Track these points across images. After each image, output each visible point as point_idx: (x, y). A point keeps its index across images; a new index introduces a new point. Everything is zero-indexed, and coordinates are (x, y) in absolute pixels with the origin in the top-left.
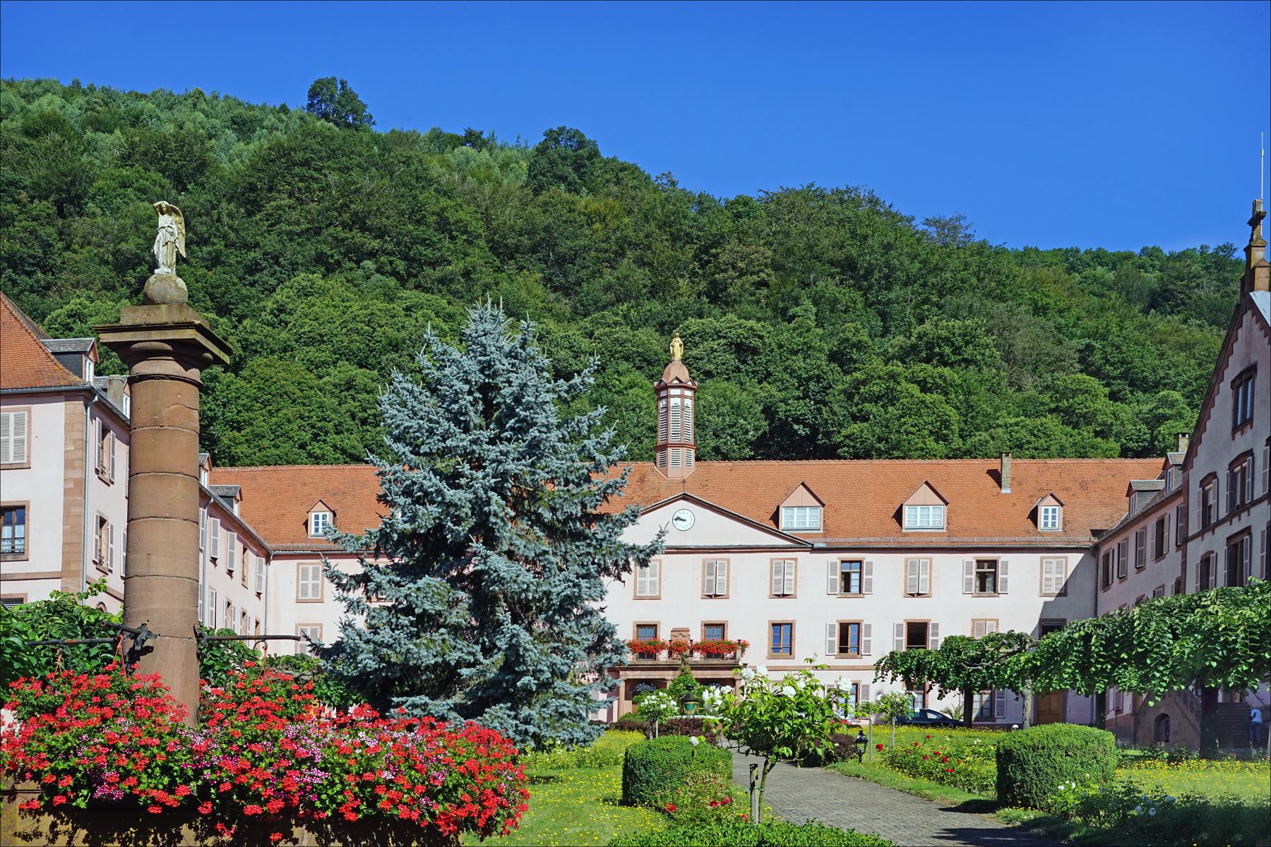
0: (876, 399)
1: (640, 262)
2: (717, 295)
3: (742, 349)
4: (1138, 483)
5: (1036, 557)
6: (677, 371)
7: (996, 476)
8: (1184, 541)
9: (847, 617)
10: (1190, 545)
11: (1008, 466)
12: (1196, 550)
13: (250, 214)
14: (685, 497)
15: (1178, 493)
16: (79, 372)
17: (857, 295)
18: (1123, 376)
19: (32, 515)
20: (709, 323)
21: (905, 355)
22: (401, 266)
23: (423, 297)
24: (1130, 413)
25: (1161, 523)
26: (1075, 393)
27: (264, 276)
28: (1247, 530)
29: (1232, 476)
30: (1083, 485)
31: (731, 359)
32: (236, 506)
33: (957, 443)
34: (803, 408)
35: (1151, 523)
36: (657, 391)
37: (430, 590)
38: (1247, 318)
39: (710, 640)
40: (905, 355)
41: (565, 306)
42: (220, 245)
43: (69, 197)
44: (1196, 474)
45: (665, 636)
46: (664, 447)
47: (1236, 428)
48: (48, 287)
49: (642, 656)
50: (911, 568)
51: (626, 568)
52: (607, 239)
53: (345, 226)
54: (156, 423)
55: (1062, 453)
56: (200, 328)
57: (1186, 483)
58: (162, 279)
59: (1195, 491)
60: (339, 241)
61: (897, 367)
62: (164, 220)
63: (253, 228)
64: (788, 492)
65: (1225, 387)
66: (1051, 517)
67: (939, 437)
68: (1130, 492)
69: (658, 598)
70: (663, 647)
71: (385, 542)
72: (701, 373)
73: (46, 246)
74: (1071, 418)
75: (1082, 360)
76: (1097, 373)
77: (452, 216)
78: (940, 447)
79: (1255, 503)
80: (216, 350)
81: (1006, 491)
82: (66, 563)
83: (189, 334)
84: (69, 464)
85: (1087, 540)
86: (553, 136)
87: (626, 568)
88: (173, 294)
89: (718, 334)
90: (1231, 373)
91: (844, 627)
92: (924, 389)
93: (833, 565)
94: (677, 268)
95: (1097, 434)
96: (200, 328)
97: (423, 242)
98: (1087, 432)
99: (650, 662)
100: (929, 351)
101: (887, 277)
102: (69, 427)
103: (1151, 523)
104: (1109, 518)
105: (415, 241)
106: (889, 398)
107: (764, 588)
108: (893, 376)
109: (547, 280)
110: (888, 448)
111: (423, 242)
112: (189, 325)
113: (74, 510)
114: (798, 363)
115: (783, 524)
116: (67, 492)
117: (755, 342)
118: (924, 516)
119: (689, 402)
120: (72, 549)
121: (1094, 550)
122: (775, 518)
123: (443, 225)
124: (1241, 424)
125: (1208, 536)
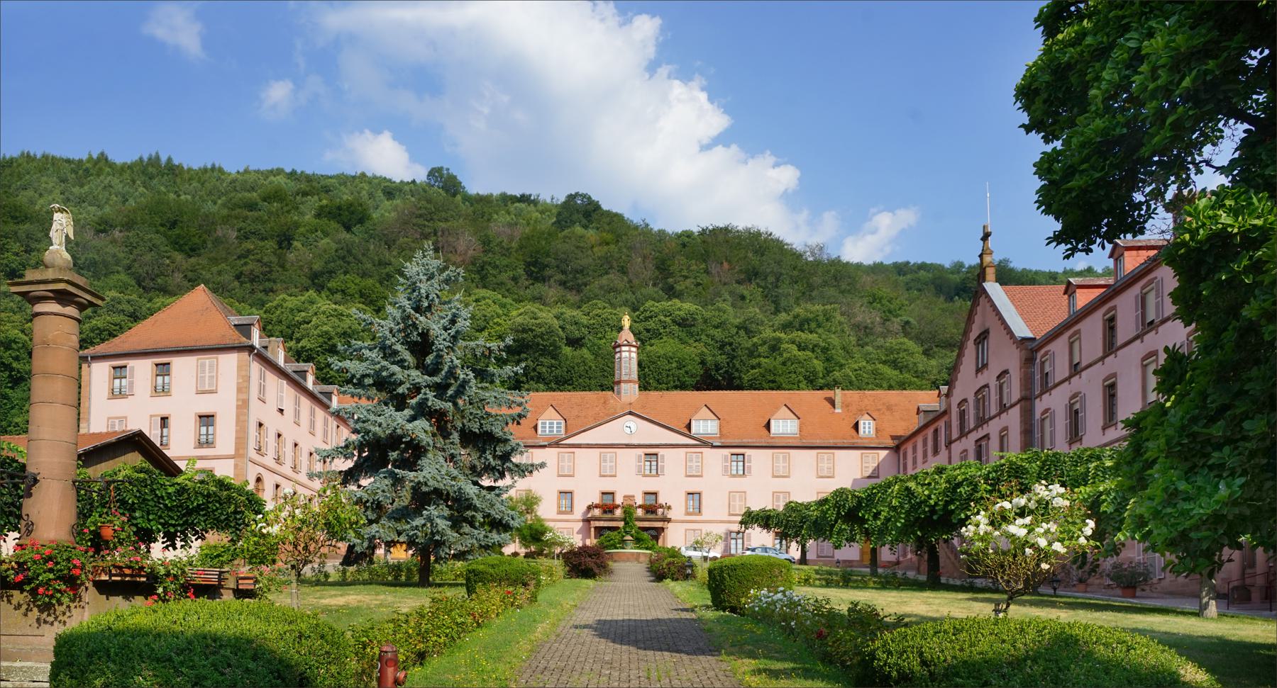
4: (924, 406)
5: (858, 452)
6: (627, 335)
7: (832, 402)
8: (949, 443)
10: (953, 445)
11: (838, 394)
12: (957, 448)
14: (631, 413)
15: (945, 413)
16: (249, 337)
19: (218, 420)
21: (786, 327)
25: (936, 431)
28: (987, 437)
29: (977, 401)
30: (889, 408)
34: (722, 359)
35: (930, 432)
36: (615, 348)
38: (982, 300)
39: (648, 503)
40: (786, 327)
41: (572, 297)
44: (955, 400)
45: (619, 501)
46: (619, 383)
47: (978, 370)
49: (647, 512)
50: (602, 459)
54: (44, 343)
56: (68, 282)
57: (949, 406)
59: (955, 411)
62: (57, 216)
64: (697, 410)
65: (970, 345)
68: (918, 412)
69: (787, 477)
70: (617, 507)
72: (643, 338)
79: (991, 419)
80: (89, 297)
81: (838, 410)
82: (237, 449)
83: (61, 286)
84: (239, 390)
85: (890, 443)
86: (571, 197)
88: (59, 262)
90: (974, 334)
92: (800, 348)
93: (726, 457)
96: (68, 282)
99: (609, 516)
102: (240, 368)
103: (930, 432)
104: (903, 429)
110: (772, 383)
113: (242, 418)
114: (718, 334)
115: (694, 430)
116: (238, 407)
118: (784, 426)
119: (634, 355)
120: (241, 441)
122: (689, 427)
124: (981, 368)
125: (964, 439)
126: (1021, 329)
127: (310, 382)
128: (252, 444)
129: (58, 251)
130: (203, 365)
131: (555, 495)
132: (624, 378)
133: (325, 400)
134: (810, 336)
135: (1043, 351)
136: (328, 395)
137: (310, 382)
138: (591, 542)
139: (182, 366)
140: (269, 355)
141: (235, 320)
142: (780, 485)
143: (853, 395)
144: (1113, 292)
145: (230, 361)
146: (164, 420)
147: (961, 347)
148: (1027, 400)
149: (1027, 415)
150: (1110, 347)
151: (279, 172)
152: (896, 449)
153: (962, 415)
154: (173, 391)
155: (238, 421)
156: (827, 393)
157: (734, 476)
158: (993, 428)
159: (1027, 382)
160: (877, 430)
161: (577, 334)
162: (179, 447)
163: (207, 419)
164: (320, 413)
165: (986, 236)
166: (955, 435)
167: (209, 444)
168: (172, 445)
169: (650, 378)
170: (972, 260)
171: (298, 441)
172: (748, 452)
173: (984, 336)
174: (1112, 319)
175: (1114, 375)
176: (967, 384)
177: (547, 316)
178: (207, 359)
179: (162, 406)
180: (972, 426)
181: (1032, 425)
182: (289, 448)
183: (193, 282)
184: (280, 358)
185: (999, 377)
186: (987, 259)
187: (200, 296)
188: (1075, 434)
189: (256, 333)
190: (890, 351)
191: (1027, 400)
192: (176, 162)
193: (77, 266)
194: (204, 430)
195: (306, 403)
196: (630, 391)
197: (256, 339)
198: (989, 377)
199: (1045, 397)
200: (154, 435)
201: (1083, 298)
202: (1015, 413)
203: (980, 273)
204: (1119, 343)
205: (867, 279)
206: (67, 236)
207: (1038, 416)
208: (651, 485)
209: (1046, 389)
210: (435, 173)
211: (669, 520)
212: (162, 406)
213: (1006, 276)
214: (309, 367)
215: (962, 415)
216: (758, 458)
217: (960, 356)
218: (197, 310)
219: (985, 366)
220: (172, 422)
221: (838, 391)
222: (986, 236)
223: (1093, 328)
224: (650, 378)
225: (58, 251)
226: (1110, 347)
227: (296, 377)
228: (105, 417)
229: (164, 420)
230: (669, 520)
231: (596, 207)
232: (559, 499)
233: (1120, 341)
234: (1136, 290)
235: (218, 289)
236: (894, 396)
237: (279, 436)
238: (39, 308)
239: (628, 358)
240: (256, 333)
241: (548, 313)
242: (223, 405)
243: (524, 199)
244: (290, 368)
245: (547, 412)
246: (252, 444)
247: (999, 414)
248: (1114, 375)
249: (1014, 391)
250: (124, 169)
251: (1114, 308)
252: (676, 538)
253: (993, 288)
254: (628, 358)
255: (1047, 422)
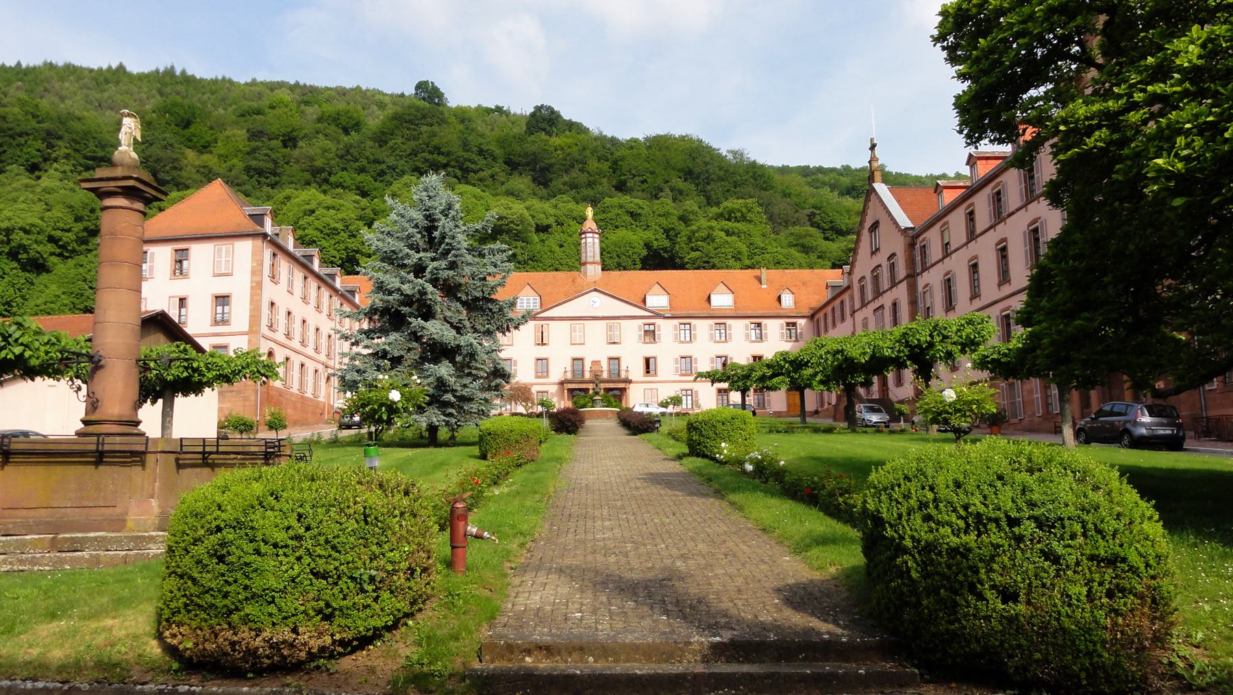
0: (704, 240)
1: (582, 170)
2: (621, 187)
3: (634, 215)
6: (590, 224)
7: (759, 279)
8: (853, 312)
9: (648, 355)
11: (764, 272)
12: (859, 316)
13: (381, 146)
14: (595, 290)
15: (848, 288)
16: (262, 225)
17: (693, 187)
18: (832, 228)
19: (233, 300)
20: (615, 201)
21: (719, 217)
22: (459, 173)
23: (470, 188)
24: (836, 247)
26: (805, 236)
27: (388, 177)
28: (882, 307)
30: (804, 284)
31: (628, 218)
32: (357, 296)
33: (748, 262)
37: (391, 341)
38: (873, 197)
41: (544, 192)
42: (364, 162)
43: (290, 140)
46: (585, 264)
47: (873, 253)
48: (276, 184)
51: (508, 330)
52: (565, 159)
53: (430, 152)
55: (801, 267)
56: (137, 179)
58: (121, 152)
60: (426, 160)
61: (714, 223)
62: (126, 121)
63: (382, 154)
65: (865, 232)
66: (788, 300)
67: (737, 259)
68: (827, 287)
69: (610, 359)
71: (371, 313)
72: (604, 225)
73: (275, 162)
74: (806, 249)
75: (810, 220)
76: (818, 227)
77: (485, 147)
78: (738, 264)
80: (154, 193)
81: (764, 286)
82: (251, 326)
83: (131, 183)
84: (253, 273)
85: (807, 312)
86: (538, 109)
87: (508, 330)
88: (127, 160)
89: (621, 207)
90: (868, 224)
91: (647, 361)
94: (600, 173)
95: (819, 257)
96: (137, 179)
97: (470, 161)
98: (813, 257)
100: (729, 216)
101: (708, 178)
105: (466, 160)
106: (709, 238)
107: (604, 339)
108: (711, 228)
109: (534, 180)
111: (470, 161)
112: (131, 178)
114: (663, 221)
116: (252, 288)
117: (640, 211)
119: (597, 241)
120: (255, 319)
121: (812, 317)
122: (644, 301)
123: (481, 152)
126: (904, 221)
127: (316, 266)
128: (264, 322)
129: (126, 151)
130: (220, 251)
131: (533, 361)
132: (590, 260)
133: (330, 281)
134: (736, 224)
135: (921, 238)
136: (332, 276)
137: (316, 266)
138: (569, 404)
139: (200, 253)
140: (280, 241)
141: (251, 210)
142: (722, 349)
143: (776, 273)
144: (972, 191)
145: (245, 248)
146: (182, 301)
147: (859, 234)
148: (912, 277)
149: (912, 289)
150: (972, 236)
151: (281, 85)
152: (812, 317)
153: (862, 289)
154: (191, 274)
155: (1007, 264)
156: (756, 272)
157: (716, 342)
158: (887, 300)
159: (911, 262)
160: (795, 303)
161: (546, 222)
162: (197, 323)
163: (222, 300)
164: (326, 293)
165: (873, 147)
166: (857, 306)
167: (224, 322)
168: (189, 323)
169: (612, 260)
170: (859, 161)
171: (306, 318)
172: (693, 322)
173: (875, 226)
174: (972, 213)
175: (976, 257)
176: (864, 265)
177: (518, 209)
178: (224, 246)
179: (181, 287)
180: (870, 298)
181: (916, 297)
182: (297, 325)
183: (208, 176)
184: (290, 245)
185: (889, 259)
186: (875, 165)
187: (217, 189)
188: (950, 306)
189: (268, 221)
190: (799, 236)
191: (912, 277)
192: (189, 73)
193: (145, 161)
194: (219, 309)
195: (313, 284)
196: (594, 271)
197: (269, 227)
198: (882, 258)
199: (925, 274)
200: (174, 314)
201: (949, 197)
202: (903, 287)
203: (870, 175)
204: (978, 231)
205: (778, 178)
206: (135, 139)
207: (920, 289)
208: (614, 351)
209: (925, 269)
210: (421, 86)
211: (630, 382)
212: (181, 287)
213: (889, 179)
214: (314, 251)
215: (862, 289)
216: (703, 327)
217: (857, 242)
218: (212, 201)
219: (878, 250)
220: (190, 303)
221: (763, 270)
222: (873, 147)
223: (957, 220)
224: (612, 260)
225: (126, 151)
226: (972, 236)
227: (304, 261)
228: (157, 295)
229: (182, 301)
230: (630, 382)
231: (558, 116)
232: (536, 365)
233: (978, 231)
234: (988, 190)
235: (231, 182)
236: (806, 273)
237: (289, 313)
238: (109, 202)
239: (592, 245)
240: (268, 221)
241: (522, 207)
242: (239, 287)
243: (499, 109)
244: (299, 253)
245: (522, 292)
246: (264, 322)
247: (891, 288)
248: (976, 257)
249: (901, 272)
250: (141, 77)
251: (972, 204)
252: (639, 400)
253: (881, 188)
254: (592, 245)
255: (928, 295)
